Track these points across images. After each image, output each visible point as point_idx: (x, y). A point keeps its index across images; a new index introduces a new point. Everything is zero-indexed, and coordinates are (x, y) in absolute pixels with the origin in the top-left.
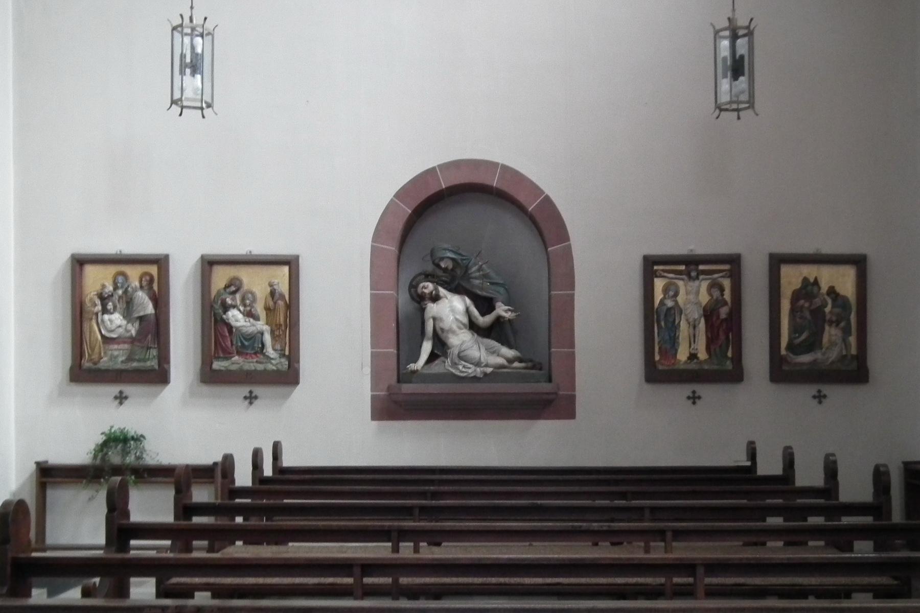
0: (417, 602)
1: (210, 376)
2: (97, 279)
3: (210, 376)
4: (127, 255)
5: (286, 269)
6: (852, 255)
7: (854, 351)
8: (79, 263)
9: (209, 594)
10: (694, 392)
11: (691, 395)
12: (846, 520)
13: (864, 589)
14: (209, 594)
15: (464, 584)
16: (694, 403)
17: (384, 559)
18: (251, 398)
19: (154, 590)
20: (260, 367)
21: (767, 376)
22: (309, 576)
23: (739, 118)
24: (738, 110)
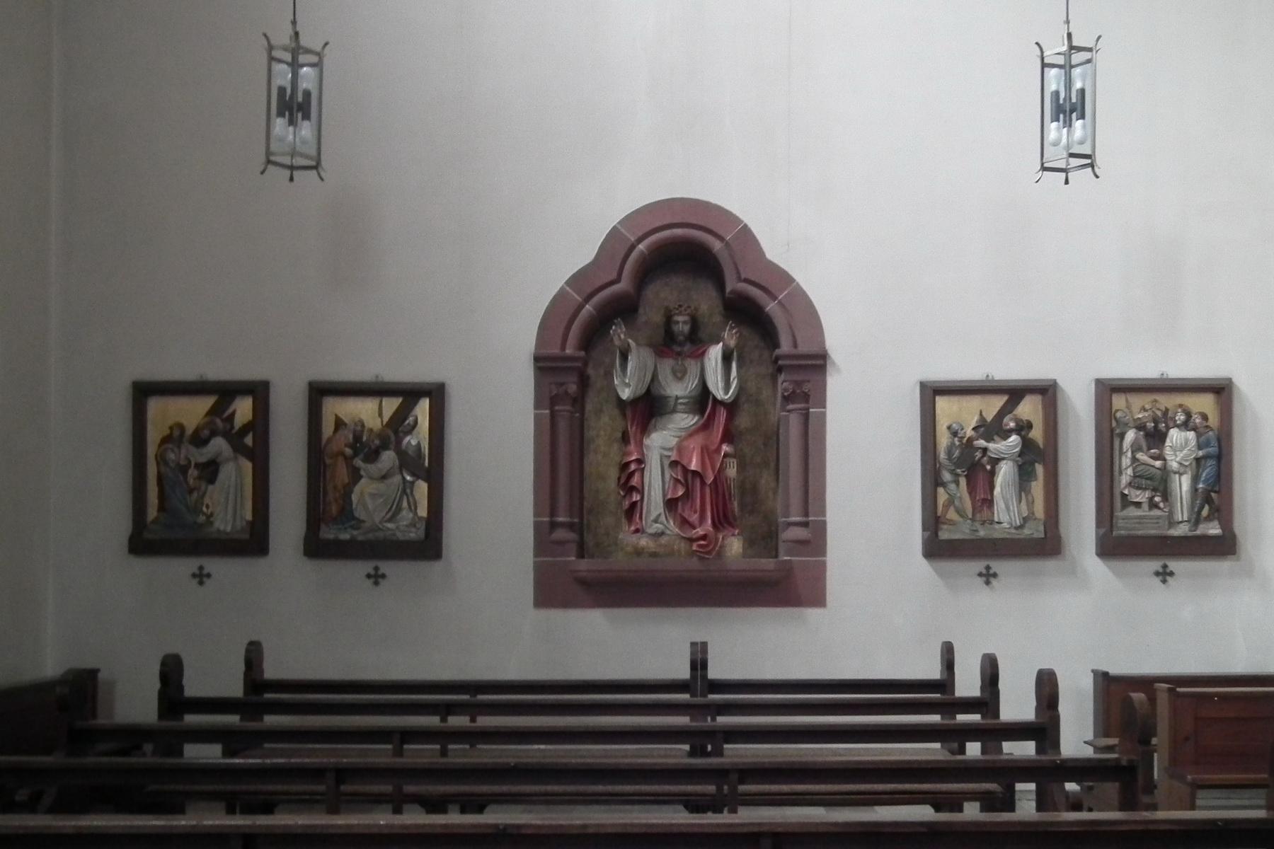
0: (271, 817)
1: (316, 548)
2: (958, 414)
3: (316, 548)
4: (388, 383)
5: (942, 403)
6: (218, 383)
7: (423, 512)
8: (932, 392)
9: (977, 805)
10: (201, 568)
11: (197, 572)
12: (962, 718)
13: (973, 796)
14: (977, 805)
15: (946, 793)
16: (201, 583)
17: (938, 762)
18: (988, 576)
19: (1034, 804)
20: (345, 536)
21: (126, 549)
22: (629, 784)
23: (291, 179)
24: (292, 168)
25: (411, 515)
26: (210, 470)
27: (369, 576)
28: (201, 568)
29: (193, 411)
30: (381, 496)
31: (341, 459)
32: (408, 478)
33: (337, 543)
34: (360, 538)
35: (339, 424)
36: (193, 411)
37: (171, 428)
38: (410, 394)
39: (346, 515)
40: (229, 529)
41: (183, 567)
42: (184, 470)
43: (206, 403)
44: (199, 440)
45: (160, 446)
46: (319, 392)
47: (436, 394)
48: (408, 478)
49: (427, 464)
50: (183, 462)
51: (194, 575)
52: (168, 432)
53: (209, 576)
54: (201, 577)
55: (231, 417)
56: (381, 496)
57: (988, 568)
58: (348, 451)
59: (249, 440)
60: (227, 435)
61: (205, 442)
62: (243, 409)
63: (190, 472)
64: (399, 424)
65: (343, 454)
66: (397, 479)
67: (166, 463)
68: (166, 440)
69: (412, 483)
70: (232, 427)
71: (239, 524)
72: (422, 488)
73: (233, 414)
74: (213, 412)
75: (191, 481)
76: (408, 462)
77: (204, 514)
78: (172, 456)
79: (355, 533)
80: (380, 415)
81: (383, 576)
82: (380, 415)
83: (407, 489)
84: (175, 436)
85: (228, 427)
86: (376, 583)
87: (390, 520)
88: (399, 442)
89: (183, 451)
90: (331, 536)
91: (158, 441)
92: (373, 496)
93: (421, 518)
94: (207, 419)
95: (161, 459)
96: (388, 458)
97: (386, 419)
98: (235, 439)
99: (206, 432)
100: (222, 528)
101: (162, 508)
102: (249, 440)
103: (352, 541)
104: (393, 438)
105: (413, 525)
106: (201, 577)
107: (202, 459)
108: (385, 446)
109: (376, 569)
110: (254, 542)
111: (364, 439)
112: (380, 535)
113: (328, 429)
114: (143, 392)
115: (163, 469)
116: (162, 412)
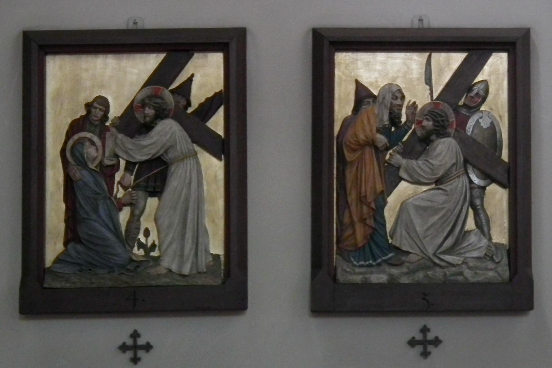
1: (329, 297)
3: (329, 297)
7: (500, 235)
10: (135, 335)
20: (379, 277)
25: (484, 242)
26: (154, 175)
27: (412, 343)
28: (135, 335)
29: (122, 79)
30: (436, 211)
31: (368, 152)
32: (476, 180)
33: (366, 287)
34: (405, 280)
35: (362, 95)
36: (122, 79)
37: (89, 106)
38: (477, 45)
39: (377, 245)
40: (186, 270)
41: (104, 334)
42: (108, 172)
43: (148, 63)
44: (135, 123)
45: (69, 135)
46: (326, 45)
47: (516, 45)
48: (476, 180)
49: (505, 156)
50: (107, 162)
51: (124, 348)
52: (82, 112)
53: (148, 347)
54: (425, 344)
55: (185, 90)
56: (436, 211)
57: (425, 330)
58: (381, 139)
59: (217, 123)
60: (180, 116)
61: (147, 128)
62: (206, 74)
63: (118, 177)
64: (463, 90)
65: (372, 144)
66: (458, 185)
67: (82, 163)
68: (75, 127)
69: (484, 188)
70: (189, 104)
71: (204, 262)
72: (497, 198)
73: (190, 80)
74: (160, 78)
75: (120, 193)
76: (480, 156)
77: (141, 245)
78: (90, 151)
79: (395, 271)
80: (428, 81)
81: (437, 342)
82: (428, 81)
83: (475, 201)
84: (92, 117)
85: (183, 102)
86: (425, 354)
87: (450, 251)
88: (462, 123)
89: (109, 143)
90: (357, 279)
91: (65, 128)
92: (423, 210)
93: (498, 246)
94: (148, 91)
95: (71, 156)
96: (446, 150)
97: (437, 90)
98: (195, 123)
99: (150, 112)
100: (174, 268)
101: (72, 235)
102: (217, 123)
103: (392, 285)
104: (452, 118)
105: (489, 257)
106: (425, 344)
107: (140, 157)
108: (441, 130)
109: (425, 330)
110: (223, 291)
111: (404, 119)
112: (438, 274)
113: (343, 106)
114: (39, 46)
115: (78, 173)
116: (72, 82)
